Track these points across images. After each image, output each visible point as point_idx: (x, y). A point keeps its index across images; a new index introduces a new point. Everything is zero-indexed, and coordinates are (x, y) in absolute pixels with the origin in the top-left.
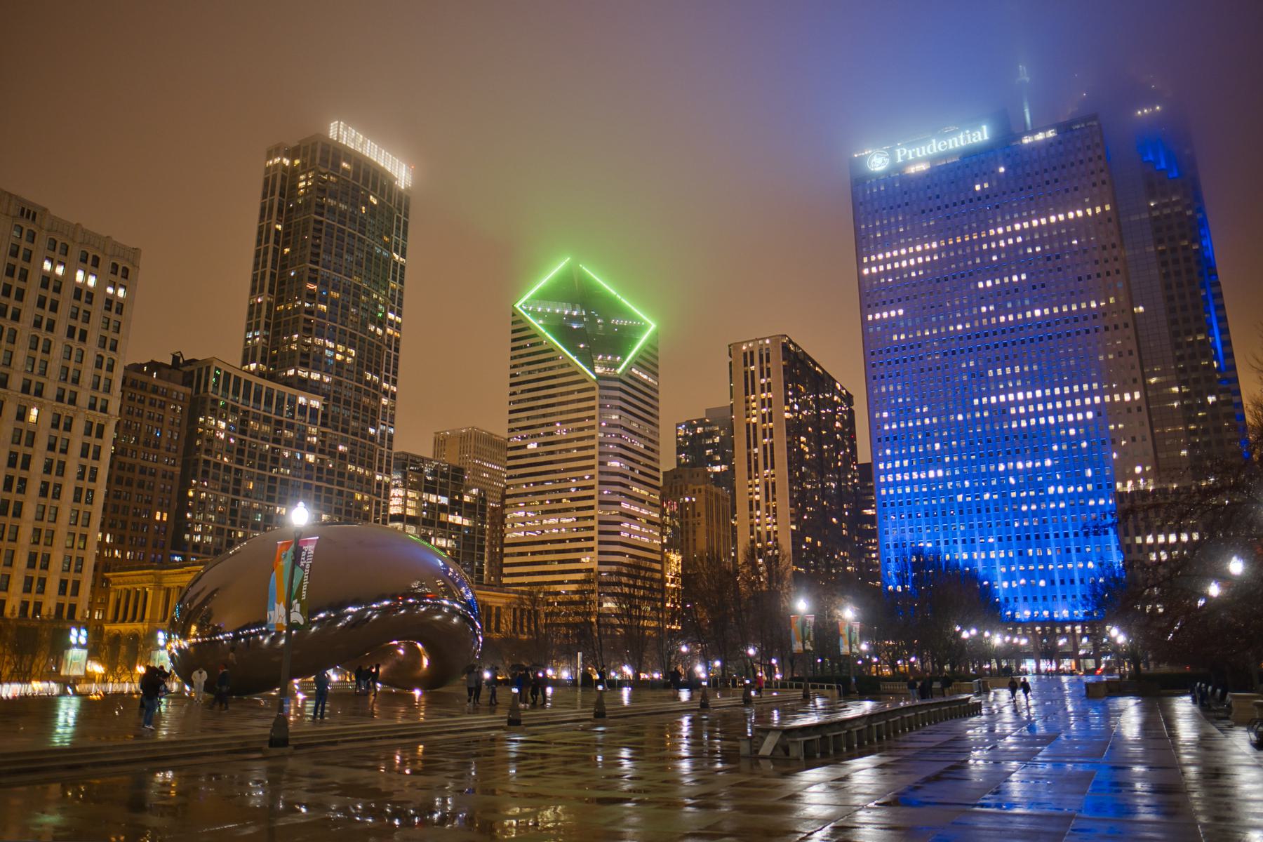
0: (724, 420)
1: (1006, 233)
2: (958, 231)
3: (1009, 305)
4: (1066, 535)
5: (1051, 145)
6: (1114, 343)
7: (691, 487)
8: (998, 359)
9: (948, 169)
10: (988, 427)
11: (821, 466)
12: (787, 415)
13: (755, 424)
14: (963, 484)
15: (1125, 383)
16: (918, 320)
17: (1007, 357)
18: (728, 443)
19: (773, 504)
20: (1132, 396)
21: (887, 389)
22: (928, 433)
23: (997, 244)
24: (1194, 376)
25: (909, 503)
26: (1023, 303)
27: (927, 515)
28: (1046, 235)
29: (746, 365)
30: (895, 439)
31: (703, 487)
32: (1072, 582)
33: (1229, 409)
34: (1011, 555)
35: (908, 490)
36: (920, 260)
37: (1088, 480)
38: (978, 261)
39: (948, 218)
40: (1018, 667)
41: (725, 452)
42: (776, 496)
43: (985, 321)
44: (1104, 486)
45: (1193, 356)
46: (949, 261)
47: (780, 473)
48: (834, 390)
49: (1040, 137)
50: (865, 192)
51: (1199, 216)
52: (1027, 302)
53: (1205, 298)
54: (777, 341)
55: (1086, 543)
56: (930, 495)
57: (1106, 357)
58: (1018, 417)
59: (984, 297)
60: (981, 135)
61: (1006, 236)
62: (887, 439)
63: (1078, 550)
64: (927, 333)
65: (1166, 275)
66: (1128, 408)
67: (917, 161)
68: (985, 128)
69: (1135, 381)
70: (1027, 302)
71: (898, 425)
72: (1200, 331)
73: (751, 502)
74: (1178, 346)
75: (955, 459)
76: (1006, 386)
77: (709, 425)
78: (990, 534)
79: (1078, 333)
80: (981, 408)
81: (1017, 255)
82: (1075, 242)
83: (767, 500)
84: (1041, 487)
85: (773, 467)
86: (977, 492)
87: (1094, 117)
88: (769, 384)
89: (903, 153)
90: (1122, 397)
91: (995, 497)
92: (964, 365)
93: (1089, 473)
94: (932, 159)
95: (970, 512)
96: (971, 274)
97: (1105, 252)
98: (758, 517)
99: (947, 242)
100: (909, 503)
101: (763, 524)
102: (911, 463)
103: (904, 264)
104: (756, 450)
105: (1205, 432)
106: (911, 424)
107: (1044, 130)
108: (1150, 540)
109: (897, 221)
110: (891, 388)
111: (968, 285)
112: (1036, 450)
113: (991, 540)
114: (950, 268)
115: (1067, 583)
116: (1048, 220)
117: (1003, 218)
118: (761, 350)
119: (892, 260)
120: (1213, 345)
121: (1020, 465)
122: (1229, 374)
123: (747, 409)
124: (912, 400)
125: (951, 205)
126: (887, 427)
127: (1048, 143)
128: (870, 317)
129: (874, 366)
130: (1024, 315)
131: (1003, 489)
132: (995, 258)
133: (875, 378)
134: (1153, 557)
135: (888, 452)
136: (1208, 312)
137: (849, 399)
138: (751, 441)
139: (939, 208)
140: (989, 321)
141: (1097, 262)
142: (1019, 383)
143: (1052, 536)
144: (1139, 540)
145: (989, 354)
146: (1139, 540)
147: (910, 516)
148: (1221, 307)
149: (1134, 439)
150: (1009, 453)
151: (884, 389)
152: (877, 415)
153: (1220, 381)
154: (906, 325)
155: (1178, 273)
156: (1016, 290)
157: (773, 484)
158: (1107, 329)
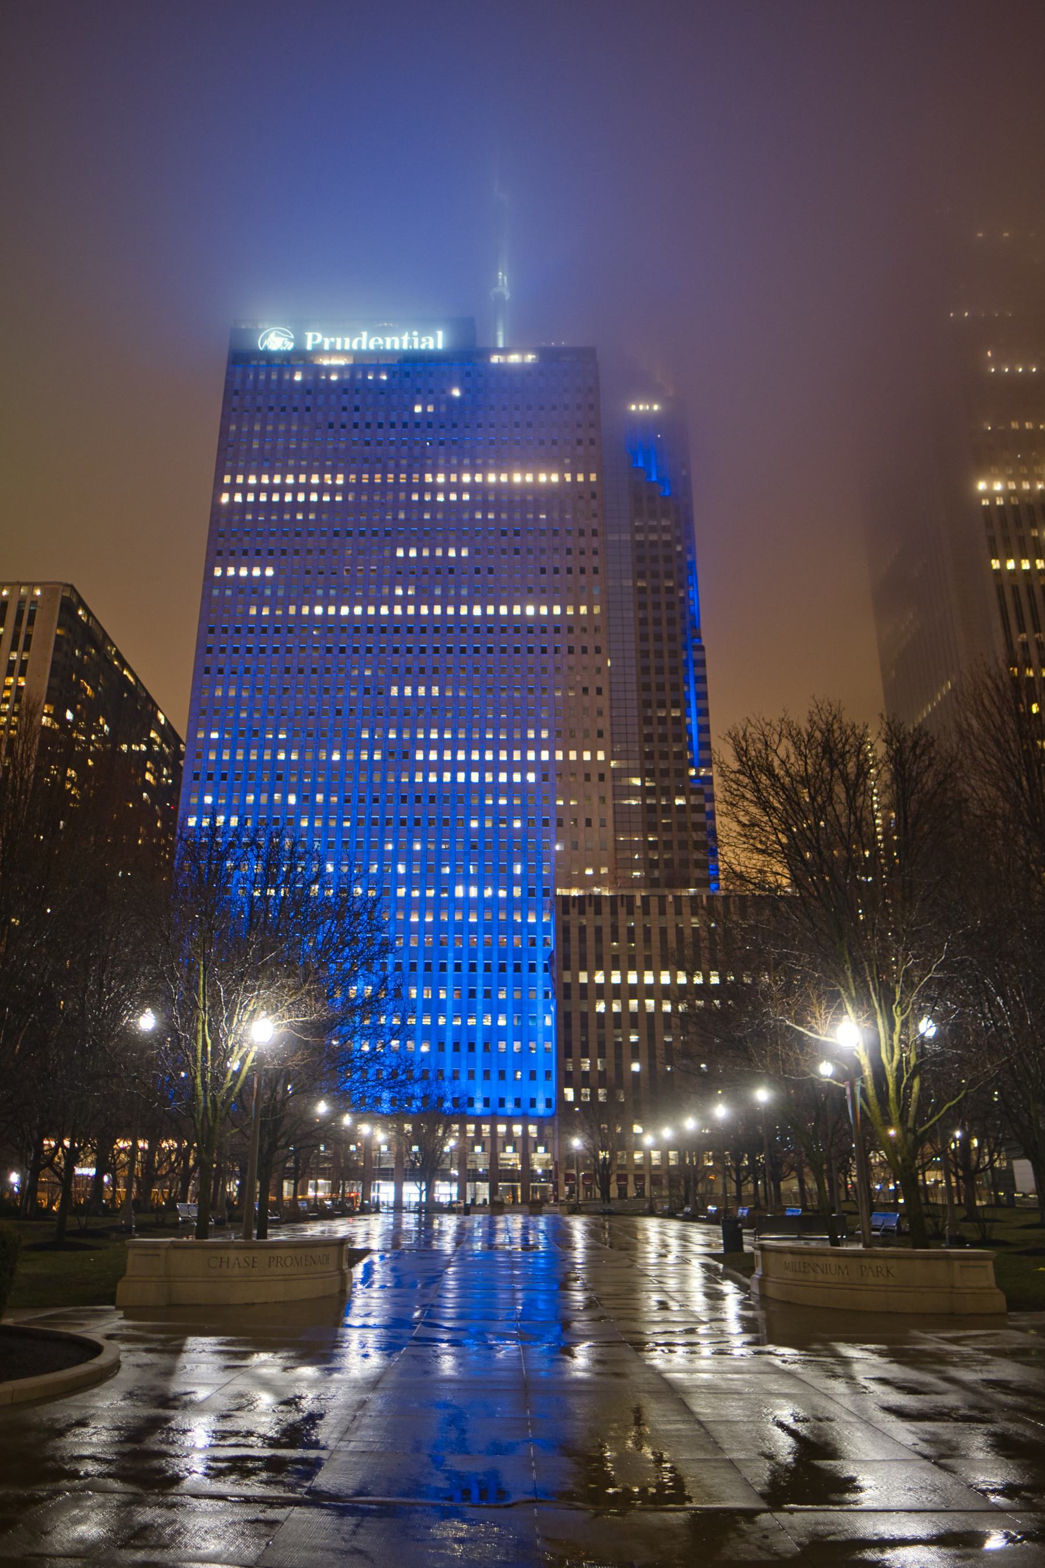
3: (438, 592)
4: (473, 967)
8: (409, 670)
17: (422, 670)
21: (226, 692)
32: (472, 1047)
33: (700, 818)
38: (402, 516)
39: (368, 443)
40: (366, 1194)
44: (536, 894)
45: (663, 738)
50: (245, 376)
51: (689, 558)
52: (464, 592)
55: (502, 983)
58: (426, 766)
59: (404, 572)
60: (435, 341)
61: (448, 488)
63: (487, 994)
65: (643, 622)
67: (333, 352)
68: (440, 334)
69: (600, 734)
70: (464, 592)
72: (676, 705)
79: (530, 650)
81: (460, 520)
82: (543, 516)
84: (444, 884)
88: (24, 663)
93: (518, 869)
94: (357, 355)
105: (668, 845)
107: (523, 351)
109: (288, 431)
111: (381, 551)
115: (464, 1048)
117: (448, 461)
119: (270, 489)
120: (688, 728)
127: (523, 370)
128: (218, 572)
129: (209, 650)
136: (687, 683)
139: (356, 426)
141: (569, 552)
143: (450, 968)
145: (396, 660)
146: (583, 977)
148: (702, 679)
154: (274, 593)
155: (657, 622)
158: (571, 650)
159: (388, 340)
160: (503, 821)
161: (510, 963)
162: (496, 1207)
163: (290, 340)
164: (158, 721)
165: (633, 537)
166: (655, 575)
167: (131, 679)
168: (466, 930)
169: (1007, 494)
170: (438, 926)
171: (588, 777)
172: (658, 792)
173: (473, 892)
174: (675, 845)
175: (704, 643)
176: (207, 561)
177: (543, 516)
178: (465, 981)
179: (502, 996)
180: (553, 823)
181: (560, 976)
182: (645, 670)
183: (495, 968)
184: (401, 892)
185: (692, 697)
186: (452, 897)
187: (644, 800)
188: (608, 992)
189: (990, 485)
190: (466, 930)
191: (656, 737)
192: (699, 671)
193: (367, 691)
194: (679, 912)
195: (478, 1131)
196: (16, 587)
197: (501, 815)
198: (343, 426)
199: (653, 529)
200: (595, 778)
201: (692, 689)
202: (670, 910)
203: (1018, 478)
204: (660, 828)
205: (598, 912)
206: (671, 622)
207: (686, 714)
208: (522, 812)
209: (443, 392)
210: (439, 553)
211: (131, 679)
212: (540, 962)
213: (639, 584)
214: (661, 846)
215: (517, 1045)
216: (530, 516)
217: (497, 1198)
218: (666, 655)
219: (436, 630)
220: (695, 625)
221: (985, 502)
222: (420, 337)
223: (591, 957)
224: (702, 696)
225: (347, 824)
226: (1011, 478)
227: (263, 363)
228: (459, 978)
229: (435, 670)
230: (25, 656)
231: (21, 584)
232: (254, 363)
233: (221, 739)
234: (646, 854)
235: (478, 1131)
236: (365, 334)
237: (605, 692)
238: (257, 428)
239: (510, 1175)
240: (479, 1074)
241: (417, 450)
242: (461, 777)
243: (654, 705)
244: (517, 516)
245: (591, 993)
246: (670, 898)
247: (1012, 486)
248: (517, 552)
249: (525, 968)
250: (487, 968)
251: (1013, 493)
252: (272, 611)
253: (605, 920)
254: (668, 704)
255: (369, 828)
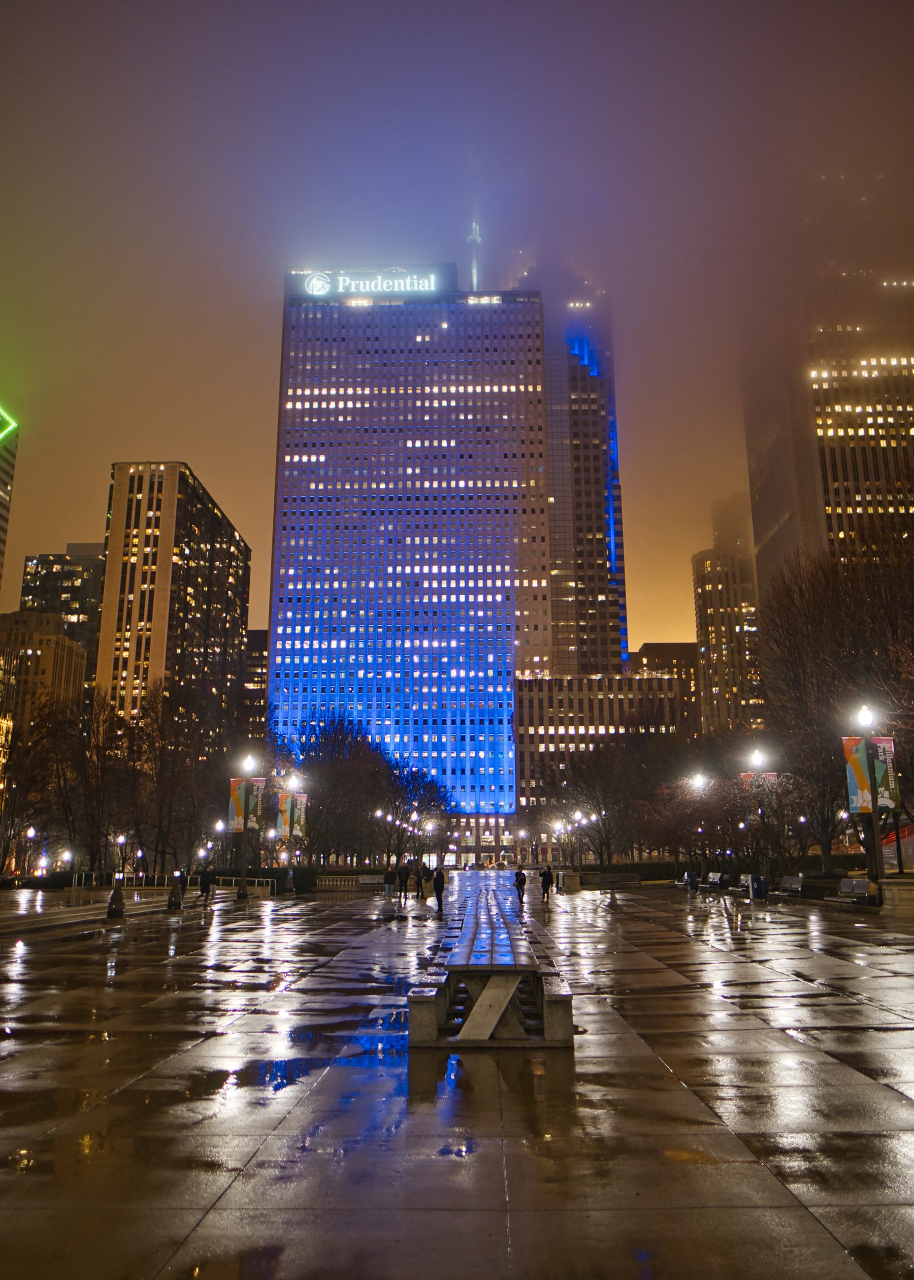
0: (92, 561)
1: (444, 393)
2: (393, 381)
3: (435, 471)
4: (463, 722)
5: (495, 312)
6: (529, 527)
7: (37, 637)
9: (392, 312)
10: (399, 598)
11: (208, 626)
12: (175, 559)
13: (133, 565)
14: (366, 659)
15: (534, 569)
16: (339, 471)
17: (426, 526)
18: (95, 587)
19: (143, 664)
20: (539, 583)
22: (335, 598)
23: (431, 403)
24: (590, 573)
25: (305, 675)
26: (449, 471)
27: (323, 690)
28: (479, 404)
29: (131, 491)
30: (299, 601)
31: (53, 638)
33: (613, 609)
34: (406, 740)
35: (306, 660)
36: (350, 404)
37: (489, 666)
38: (410, 417)
39: (385, 365)
41: (92, 591)
42: (149, 655)
43: (409, 484)
44: (504, 673)
45: (590, 554)
46: (380, 411)
47: (158, 629)
48: (231, 541)
49: (485, 300)
51: (611, 418)
52: (453, 471)
53: (607, 498)
54: (174, 468)
55: (482, 732)
56: (329, 668)
57: (520, 540)
58: (431, 591)
59: (412, 457)
60: (428, 284)
62: (290, 600)
63: (472, 738)
64: (348, 487)
65: (577, 470)
66: (535, 595)
67: (358, 295)
70: (453, 471)
71: (304, 585)
72: (599, 530)
73: (117, 660)
74: (580, 542)
75: (362, 630)
76: (422, 556)
77: (69, 563)
78: (388, 716)
79: (498, 511)
80: (395, 577)
81: (449, 420)
82: (505, 417)
83: (138, 658)
85: (150, 620)
86: (379, 669)
87: (537, 294)
88: (157, 519)
89: (344, 282)
90: (530, 583)
91: (398, 675)
92: (382, 528)
93: (491, 658)
94: (377, 297)
95: (370, 690)
96: (401, 430)
97: (532, 433)
98: (124, 679)
99: (380, 391)
100: (305, 675)
101: (129, 688)
102: (313, 630)
103: (332, 405)
104: (131, 597)
105: (593, 629)
106: (318, 586)
107: (490, 294)
108: (541, 731)
109: (330, 355)
110: (302, 542)
111: (397, 441)
112: (444, 628)
113: (387, 723)
114: (380, 420)
115: (458, 772)
116: (483, 389)
117: (440, 377)
118: (152, 476)
119: (320, 398)
120: (608, 546)
121: (426, 644)
122: (618, 576)
123: (126, 545)
124: (323, 560)
125: (389, 352)
126: (291, 587)
127: (491, 309)
128: (288, 459)
130: (449, 484)
131: (406, 669)
132: (427, 418)
133: (284, 528)
134: (542, 748)
135: (290, 614)
136: (608, 513)
137: (246, 552)
138: (128, 584)
140: (413, 484)
142: (435, 556)
143: (449, 722)
144: (531, 731)
146: (531, 731)
147: (305, 690)
148: (618, 510)
149: (536, 628)
150: (417, 629)
151: (293, 543)
152: (283, 571)
153: (610, 581)
154: (326, 474)
155: (587, 470)
156: (444, 457)
157: (148, 640)
158: (524, 511)
159: (396, 282)
160: (481, 627)
161: (486, 718)
162: (479, 866)
163: (327, 283)
164: (235, 538)
165: (572, 442)
166: (586, 435)
167: (219, 514)
168: (458, 698)
169: (831, 380)
170: (440, 696)
171: (535, 598)
172: (587, 592)
173: (463, 673)
174: (598, 628)
175: (620, 483)
176: (278, 451)
177: (505, 417)
178: (458, 730)
179: (481, 738)
180: (513, 628)
181: (517, 730)
182: (578, 505)
183: (477, 722)
184: (417, 674)
185: (612, 523)
186: (449, 678)
187: (577, 598)
188: (547, 739)
189: (819, 374)
190: (458, 698)
191: (585, 554)
192: (616, 504)
193: (390, 541)
194: (590, 689)
195: (468, 823)
196: (148, 466)
197: (480, 623)
198: (368, 352)
199: (585, 401)
200: (540, 598)
201: (610, 517)
202: (585, 688)
203: (839, 368)
204: (588, 617)
205: (541, 690)
206: (597, 470)
207: (607, 535)
208: (493, 621)
209: (436, 326)
210: (436, 443)
211: (219, 514)
212: (505, 719)
213: (575, 442)
214: (588, 630)
215: (491, 770)
216: (497, 417)
217: (480, 863)
218: (593, 494)
219: (435, 498)
220: (614, 469)
221: (815, 387)
222: (418, 279)
223: (536, 719)
224: (618, 522)
225: (380, 630)
226: (834, 368)
227: (311, 305)
228: (455, 728)
229: (435, 526)
230: (158, 513)
231: (151, 463)
232: (304, 305)
233: (295, 575)
234: (578, 635)
235: (468, 823)
236: (380, 278)
237: (547, 540)
238: (309, 354)
239: (488, 849)
240: (468, 788)
241: (419, 369)
242: (453, 569)
243: (585, 530)
244: (488, 417)
245: (536, 740)
246: (585, 681)
247: (835, 374)
248: (488, 442)
249: (496, 722)
250: (472, 722)
251: (834, 379)
252: (325, 486)
253: (545, 695)
254: (594, 529)
255: (394, 633)
